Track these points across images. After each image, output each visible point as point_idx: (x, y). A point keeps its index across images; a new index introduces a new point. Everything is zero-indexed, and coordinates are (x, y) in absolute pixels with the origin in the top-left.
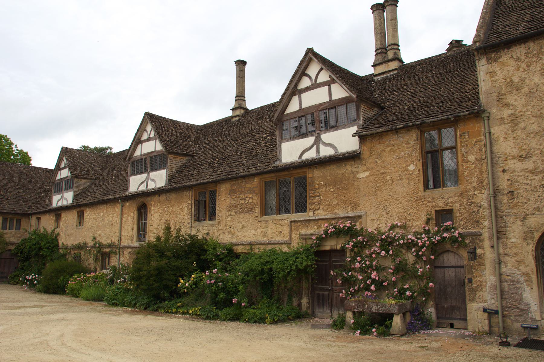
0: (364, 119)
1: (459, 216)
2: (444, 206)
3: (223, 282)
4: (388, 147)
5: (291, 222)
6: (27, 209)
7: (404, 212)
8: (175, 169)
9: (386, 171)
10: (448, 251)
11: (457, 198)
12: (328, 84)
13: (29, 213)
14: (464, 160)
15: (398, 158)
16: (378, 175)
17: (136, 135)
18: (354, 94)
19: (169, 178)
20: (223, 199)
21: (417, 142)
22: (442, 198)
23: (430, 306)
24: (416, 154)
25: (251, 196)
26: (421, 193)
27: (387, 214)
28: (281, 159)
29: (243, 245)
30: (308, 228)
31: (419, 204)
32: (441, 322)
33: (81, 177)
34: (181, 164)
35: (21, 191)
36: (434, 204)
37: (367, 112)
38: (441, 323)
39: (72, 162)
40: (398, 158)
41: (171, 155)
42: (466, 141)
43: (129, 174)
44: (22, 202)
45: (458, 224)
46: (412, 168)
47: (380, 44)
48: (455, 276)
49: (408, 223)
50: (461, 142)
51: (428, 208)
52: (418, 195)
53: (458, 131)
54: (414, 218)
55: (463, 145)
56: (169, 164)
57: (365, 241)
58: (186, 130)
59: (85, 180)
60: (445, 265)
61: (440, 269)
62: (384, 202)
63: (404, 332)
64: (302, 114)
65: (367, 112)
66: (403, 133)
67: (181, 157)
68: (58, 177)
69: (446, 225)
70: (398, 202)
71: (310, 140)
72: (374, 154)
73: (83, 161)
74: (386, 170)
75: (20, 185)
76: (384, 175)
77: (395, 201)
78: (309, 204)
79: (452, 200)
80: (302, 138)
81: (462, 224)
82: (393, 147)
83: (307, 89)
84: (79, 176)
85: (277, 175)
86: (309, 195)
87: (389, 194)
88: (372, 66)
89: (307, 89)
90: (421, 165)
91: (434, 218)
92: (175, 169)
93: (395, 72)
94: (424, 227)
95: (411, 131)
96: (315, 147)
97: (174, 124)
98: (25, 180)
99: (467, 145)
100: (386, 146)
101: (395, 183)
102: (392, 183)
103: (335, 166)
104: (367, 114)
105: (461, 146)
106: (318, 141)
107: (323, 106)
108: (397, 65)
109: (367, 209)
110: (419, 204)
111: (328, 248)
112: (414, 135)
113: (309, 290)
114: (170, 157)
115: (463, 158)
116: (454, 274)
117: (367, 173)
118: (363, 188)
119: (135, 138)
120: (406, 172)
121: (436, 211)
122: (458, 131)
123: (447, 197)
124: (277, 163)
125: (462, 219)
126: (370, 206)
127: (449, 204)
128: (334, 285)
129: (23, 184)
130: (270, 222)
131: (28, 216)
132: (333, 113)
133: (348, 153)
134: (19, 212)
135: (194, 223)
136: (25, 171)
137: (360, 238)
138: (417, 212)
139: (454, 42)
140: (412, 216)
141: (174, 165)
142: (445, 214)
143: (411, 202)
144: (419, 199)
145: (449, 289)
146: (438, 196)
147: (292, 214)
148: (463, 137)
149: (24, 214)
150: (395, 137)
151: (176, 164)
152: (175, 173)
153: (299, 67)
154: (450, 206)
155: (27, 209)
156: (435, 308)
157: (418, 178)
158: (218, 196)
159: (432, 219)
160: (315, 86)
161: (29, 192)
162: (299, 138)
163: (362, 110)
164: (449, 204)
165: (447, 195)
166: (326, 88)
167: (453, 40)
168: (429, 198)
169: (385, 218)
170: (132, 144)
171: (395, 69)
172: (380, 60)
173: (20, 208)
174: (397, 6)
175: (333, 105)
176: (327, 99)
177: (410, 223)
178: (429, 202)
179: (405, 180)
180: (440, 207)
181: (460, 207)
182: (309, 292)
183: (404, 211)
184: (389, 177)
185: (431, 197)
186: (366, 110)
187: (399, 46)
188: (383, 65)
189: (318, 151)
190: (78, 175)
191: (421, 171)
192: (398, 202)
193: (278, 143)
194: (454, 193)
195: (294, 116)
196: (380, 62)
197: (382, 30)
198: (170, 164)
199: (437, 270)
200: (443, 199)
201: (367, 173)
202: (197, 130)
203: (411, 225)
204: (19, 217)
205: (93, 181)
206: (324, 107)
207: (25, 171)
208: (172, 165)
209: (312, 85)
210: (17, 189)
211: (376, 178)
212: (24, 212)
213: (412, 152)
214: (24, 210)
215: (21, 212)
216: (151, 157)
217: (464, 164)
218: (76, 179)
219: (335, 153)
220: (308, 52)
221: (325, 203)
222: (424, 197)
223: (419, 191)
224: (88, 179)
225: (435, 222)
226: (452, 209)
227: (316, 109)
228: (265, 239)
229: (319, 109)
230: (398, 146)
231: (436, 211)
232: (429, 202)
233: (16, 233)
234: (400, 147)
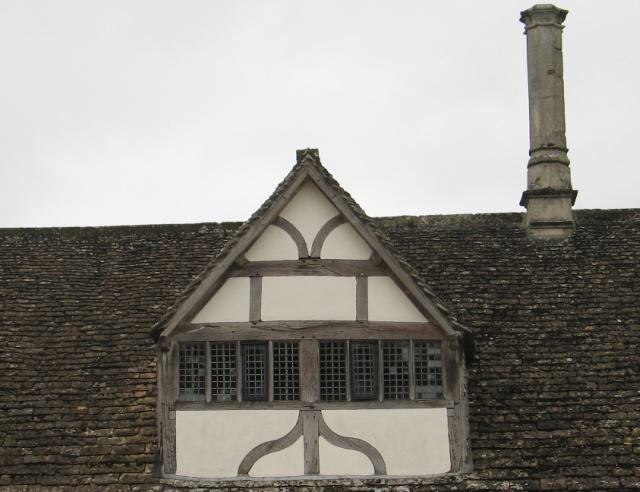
71: (279, 420)
160: (308, 264)
176: (350, 314)
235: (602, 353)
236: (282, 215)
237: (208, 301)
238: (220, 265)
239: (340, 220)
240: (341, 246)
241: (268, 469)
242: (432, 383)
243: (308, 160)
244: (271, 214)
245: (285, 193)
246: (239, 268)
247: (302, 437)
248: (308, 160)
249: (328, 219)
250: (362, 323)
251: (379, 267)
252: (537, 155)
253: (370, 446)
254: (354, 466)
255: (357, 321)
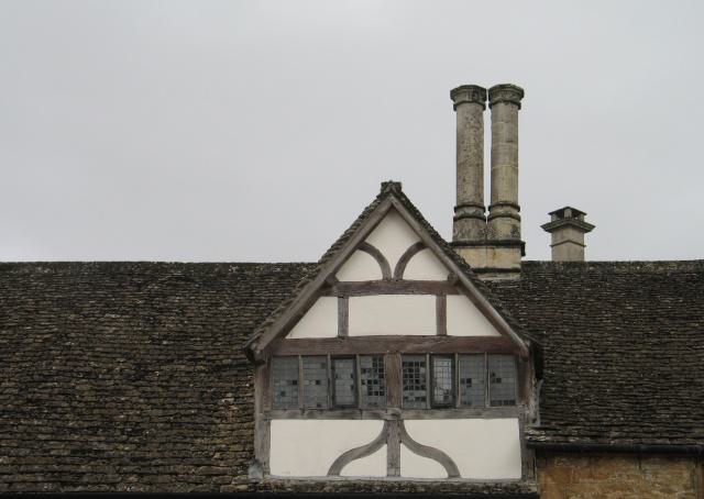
4: (614, 491)
18: (524, 339)
21: (692, 491)
28: (267, 463)
64: (345, 351)
71: (370, 429)
80: (343, 417)
82: (628, 493)
83: (368, 288)
89: (368, 288)
93: (515, 277)
96: (404, 450)
100: (610, 488)
106: (394, 435)
107: (417, 346)
112: (686, 474)
124: (254, 474)
132: (446, 375)
133: (497, 484)
139: (568, 214)
153: (357, 225)
160: (394, 284)
162: (330, 413)
166: (431, 300)
167: (568, 208)
171: (515, 271)
172: (472, 234)
174: (519, 107)
175: (447, 347)
176: (431, 330)
187: (518, 209)
188: (483, 251)
189: (394, 463)
193: (258, 415)
195: (318, 350)
196: (471, 239)
206: (419, 349)
209: (387, 280)
219: (450, 476)
230: (642, 492)
235: (77, 364)
236: (367, 241)
237: (298, 321)
238: (312, 283)
239: (420, 246)
240: (423, 268)
241: (356, 471)
242: (376, 393)
243: (392, 191)
244: (356, 240)
245: (370, 219)
246: (326, 289)
247: (386, 446)
248: (392, 191)
249: (410, 245)
250: (342, 338)
251: (455, 286)
252: (461, 213)
253: (414, 451)
254: (432, 472)
255: (339, 337)
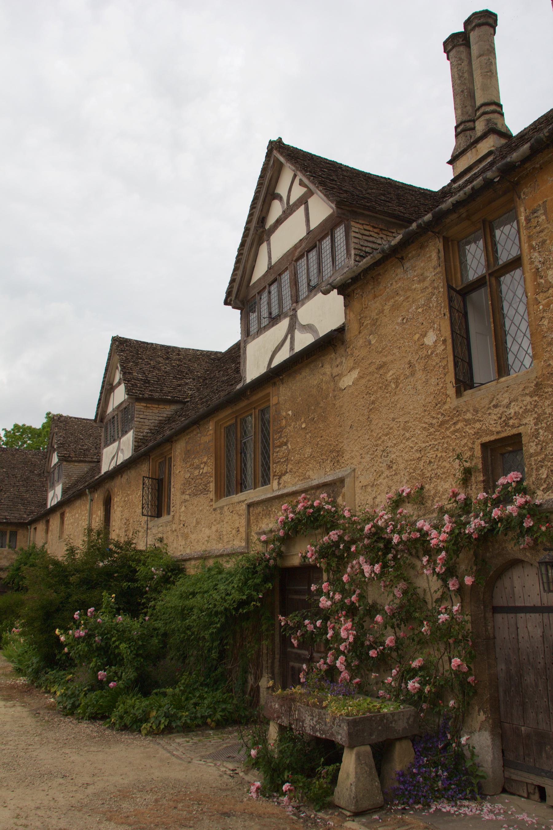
0: (358, 252)
1: (537, 454)
2: (499, 429)
3: (102, 634)
5: (249, 506)
6: (25, 516)
7: (419, 459)
8: (147, 427)
9: (384, 359)
10: (516, 563)
11: (528, 399)
12: (303, 201)
13: (26, 521)
14: (539, 284)
15: (405, 321)
16: (372, 374)
17: (105, 377)
19: (136, 444)
20: (177, 472)
22: (496, 406)
23: (477, 726)
24: (437, 301)
25: (205, 460)
26: (453, 402)
27: (389, 467)
29: (196, 559)
30: (270, 517)
31: (448, 433)
32: (514, 777)
33: (74, 459)
34: (160, 418)
35: (22, 489)
36: (478, 425)
37: (371, 239)
38: (515, 781)
39: (64, 438)
40: (405, 321)
41: (140, 402)
42: (541, 231)
43: (102, 445)
44: (20, 506)
45: (533, 478)
46: (430, 339)
47: (462, 114)
48: (543, 636)
49: (427, 486)
50: (530, 238)
51: (465, 441)
52: (446, 407)
53: (522, 209)
54: (440, 471)
55: (534, 243)
56: (135, 419)
57: (344, 541)
58: (189, 360)
59: (81, 464)
60: (519, 604)
61: (505, 615)
62: (383, 438)
63: (365, 805)
65: (371, 239)
66: (413, 257)
67: (161, 406)
68: (53, 465)
69: (505, 481)
70: (407, 435)
72: (367, 325)
73: (83, 435)
74: (386, 356)
75: (22, 481)
76: (381, 372)
77: (402, 432)
78: (274, 463)
79: (517, 409)
81: (544, 476)
82: (397, 298)
84: (70, 459)
85: (234, 410)
86: (274, 444)
87: (392, 416)
88: (450, 162)
90: (449, 328)
91: (480, 466)
92: (147, 427)
94: (455, 495)
95: (427, 246)
97: (168, 353)
98: (32, 472)
99: (544, 242)
101: (401, 385)
102: (397, 387)
103: (307, 370)
104: (373, 242)
105: (532, 247)
108: (492, 144)
109: (355, 462)
110: (448, 433)
111: (296, 561)
113: (273, 659)
114: (139, 406)
115: (535, 280)
116: (539, 632)
117: (355, 374)
118: (348, 412)
119: (104, 382)
120: (420, 353)
121: (484, 446)
122: (522, 209)
123: (506, 401)
125: (543, 460)
126: (361, 452)
127: (511, 422)
128: (315, 650)
129: (28, 478)
130: (226, 508)
131: (25, 525)
134: (12, 521)
135: (150, 521)
136: (33, 459)
137: (334, 535)
138: (444, 454)
140: (435, 467)
141: (146, 421)
142: (510, 452)
143: (432, 430)
144: (447, 418)
145: (530, 678)
146: (485, 402)
147: (255, 488)
148: (534, 222)
149: (20, 523)
150: (400, 271)
151: (151, 418)
152: (149, 435)
154: (513, 426)
155: (25, 516)
156: (493, 733)
157: (444, 363)
158: (174, 466)
159: (475, 469)
161: (34, 490)
163: (353, 234)
164: (511, 422)
165: (506, 395)
168: (468, 411)
169: (386, 480)
170: (101, 393)
173: (16, 515)
177: (432, 485)
178: (468, 422)
179: (420, 375)
180: (492, 433)
181: (536, 424)
182: (273, 663)
183: (418, 455)
184: (391, 373)
185: (471, 409)
186: (367, 233)
187: (500, 106)
190: (69, 457)
191: (449, 341)
192: (407, 435)
194: (522, 387)
197: (465, 84)
198: (138, 419)
199: (499, 617)
200: (498, 409)
201: (355, 374)
202: (214, 360)
203: (432, 492)
204: (14, 529)
205: (94, 465)
206: (300, 252)
207: (33, 459)
208: (142, 420)
210: (18, 486)
211: (369, 381)
212: (19, 521)
213: (429, 300)
214: (21, 518)
215: (16, 521)
216: (121, 411)
217: (540, 297)
218: (65, 463)
220: (272, 148)
221: (294, 456)
222: (458, 411)
223: (447, 396)
224: (85, 462)
225: (481, 478)
226: (519, 435)
227: (290, 258)
228: (220, 546)
229: (294, 259)
231: (484, 446)
232: (468, 422)
233: (9, 553)
234: (409, 294)
